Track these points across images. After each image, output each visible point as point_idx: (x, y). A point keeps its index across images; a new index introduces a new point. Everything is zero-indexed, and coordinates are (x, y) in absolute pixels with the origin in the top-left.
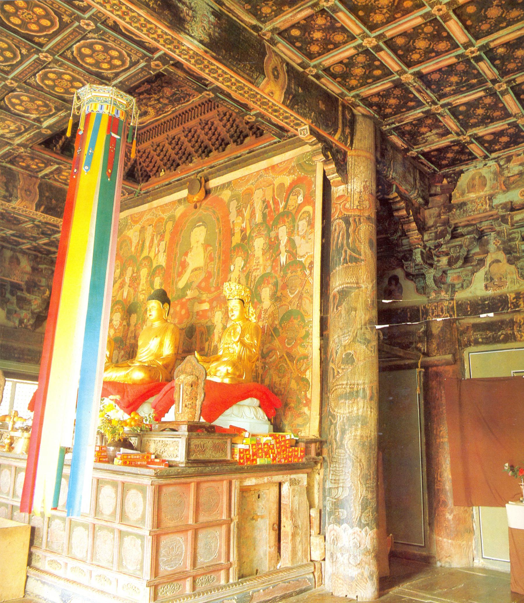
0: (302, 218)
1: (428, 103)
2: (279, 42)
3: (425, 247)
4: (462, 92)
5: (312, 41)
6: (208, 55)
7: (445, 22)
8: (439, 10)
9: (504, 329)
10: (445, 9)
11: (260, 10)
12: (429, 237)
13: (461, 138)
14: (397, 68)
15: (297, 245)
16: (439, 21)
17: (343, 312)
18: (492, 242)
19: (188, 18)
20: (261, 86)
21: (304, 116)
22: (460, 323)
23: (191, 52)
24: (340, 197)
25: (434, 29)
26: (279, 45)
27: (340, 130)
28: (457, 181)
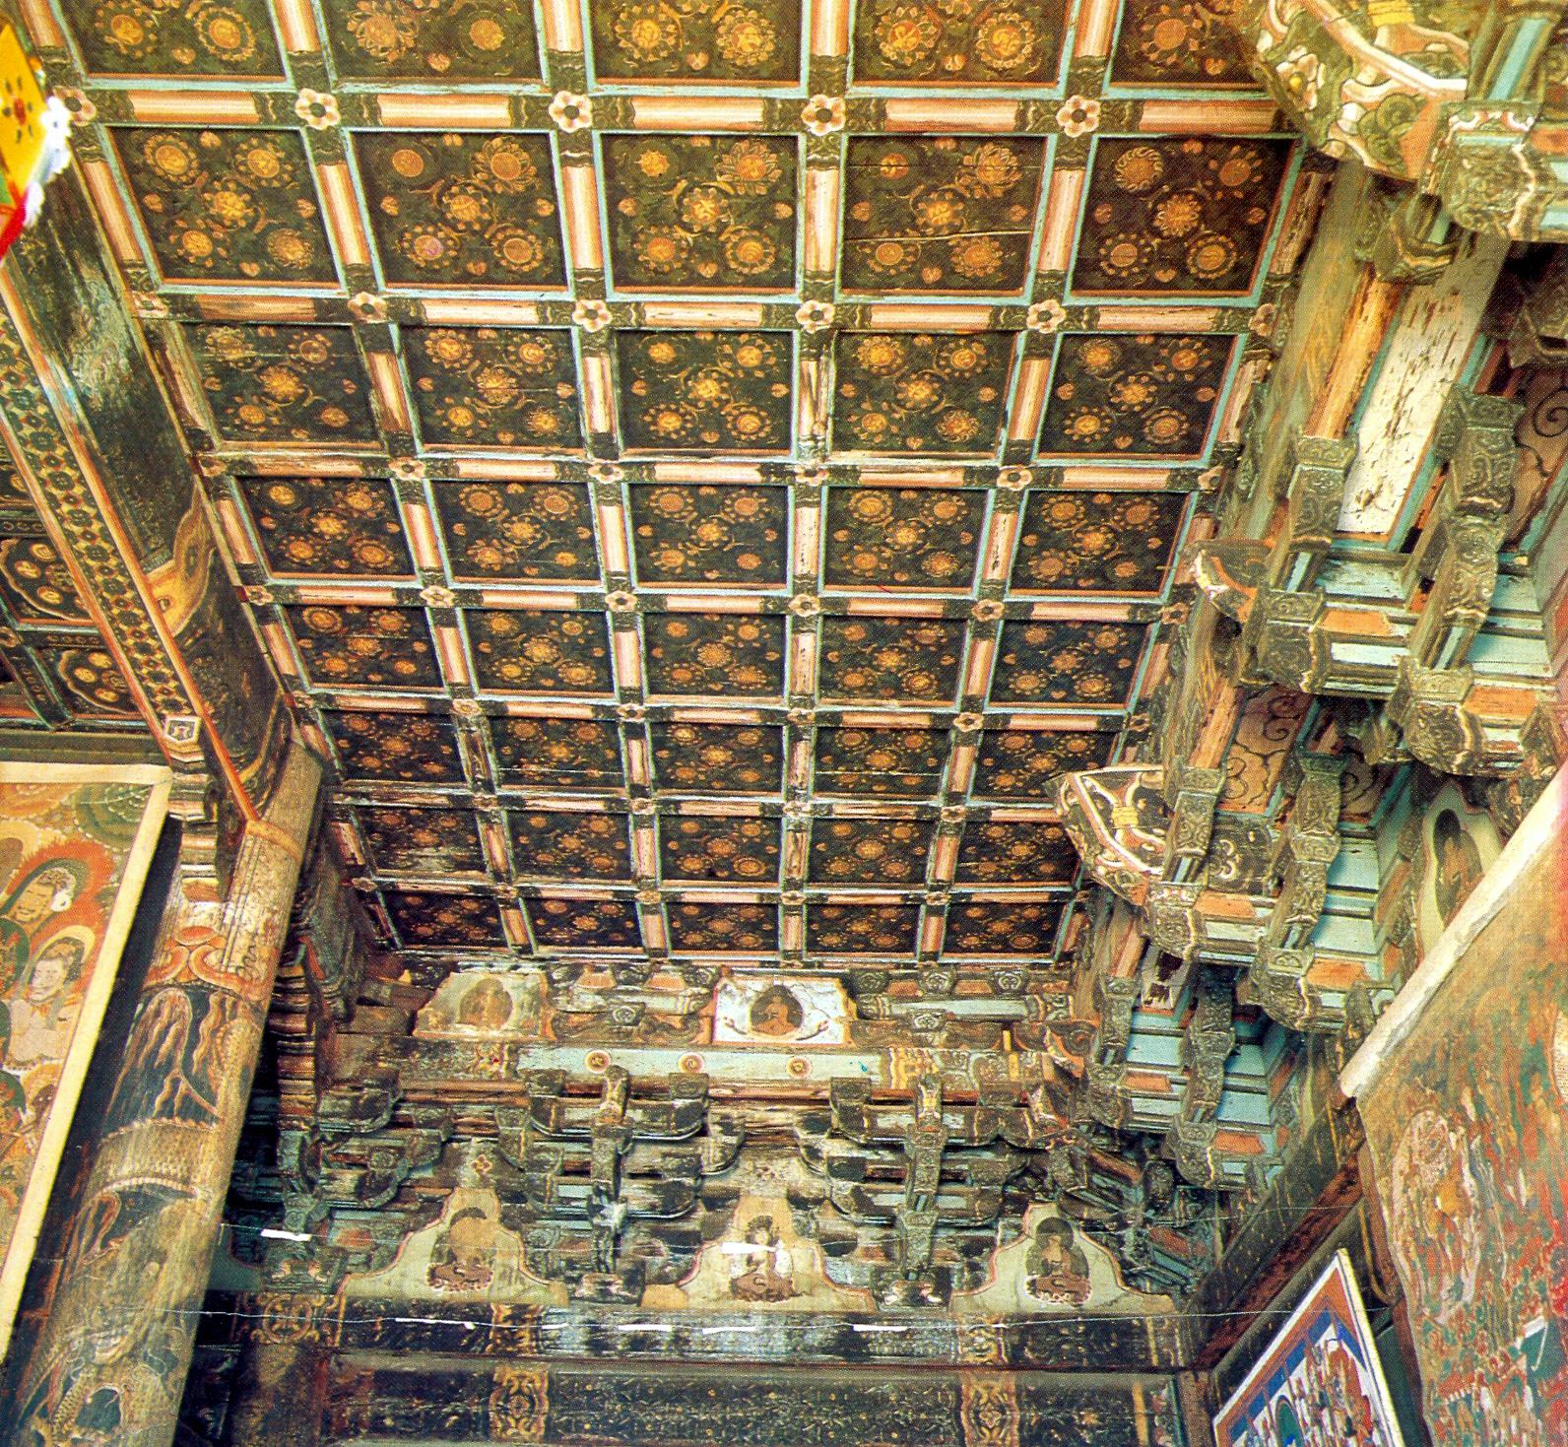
0: (52, 952)
1: (475, 780)
2: (230, 496)
3: (315, 1129)
4: (558, 787)
5: (309, 533)
6: (82, 438)
7: (616, 629)
8: (621, 601)
9: (461, 1400)
10: (632, 603)
11: (238, 406)
12: (334, 1106)
13: (500, 887)
14: (458, 677)
15: (15, 1029)
16: (605, 623)
17: (123, 1259)
18: (470, 1160)
19: (83, 333)
20: (152, 576)
21: (205, 691)
22: (340, 1365)
23: (42, 410)
24: (194, 931)
25: (584, 632)
26: (226, 504)
27: (258, 762)
28: (437, 984)
